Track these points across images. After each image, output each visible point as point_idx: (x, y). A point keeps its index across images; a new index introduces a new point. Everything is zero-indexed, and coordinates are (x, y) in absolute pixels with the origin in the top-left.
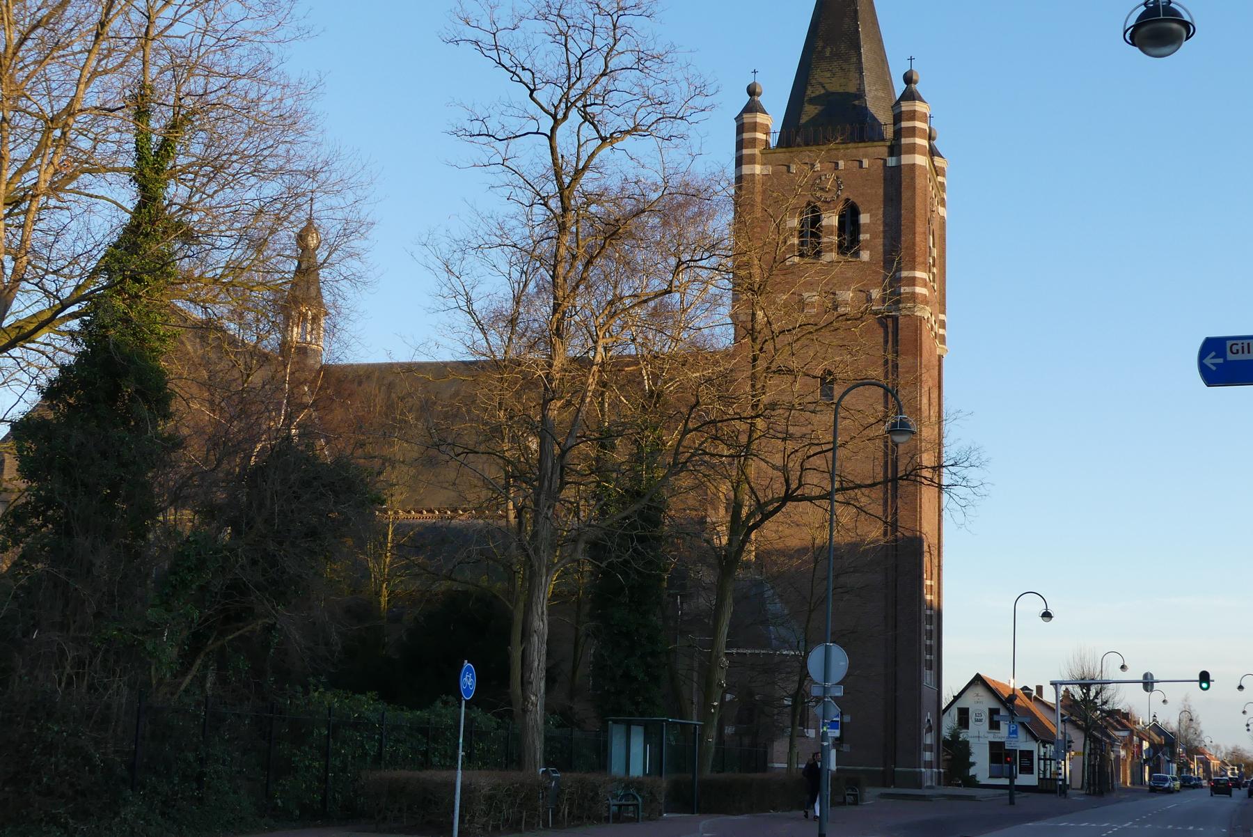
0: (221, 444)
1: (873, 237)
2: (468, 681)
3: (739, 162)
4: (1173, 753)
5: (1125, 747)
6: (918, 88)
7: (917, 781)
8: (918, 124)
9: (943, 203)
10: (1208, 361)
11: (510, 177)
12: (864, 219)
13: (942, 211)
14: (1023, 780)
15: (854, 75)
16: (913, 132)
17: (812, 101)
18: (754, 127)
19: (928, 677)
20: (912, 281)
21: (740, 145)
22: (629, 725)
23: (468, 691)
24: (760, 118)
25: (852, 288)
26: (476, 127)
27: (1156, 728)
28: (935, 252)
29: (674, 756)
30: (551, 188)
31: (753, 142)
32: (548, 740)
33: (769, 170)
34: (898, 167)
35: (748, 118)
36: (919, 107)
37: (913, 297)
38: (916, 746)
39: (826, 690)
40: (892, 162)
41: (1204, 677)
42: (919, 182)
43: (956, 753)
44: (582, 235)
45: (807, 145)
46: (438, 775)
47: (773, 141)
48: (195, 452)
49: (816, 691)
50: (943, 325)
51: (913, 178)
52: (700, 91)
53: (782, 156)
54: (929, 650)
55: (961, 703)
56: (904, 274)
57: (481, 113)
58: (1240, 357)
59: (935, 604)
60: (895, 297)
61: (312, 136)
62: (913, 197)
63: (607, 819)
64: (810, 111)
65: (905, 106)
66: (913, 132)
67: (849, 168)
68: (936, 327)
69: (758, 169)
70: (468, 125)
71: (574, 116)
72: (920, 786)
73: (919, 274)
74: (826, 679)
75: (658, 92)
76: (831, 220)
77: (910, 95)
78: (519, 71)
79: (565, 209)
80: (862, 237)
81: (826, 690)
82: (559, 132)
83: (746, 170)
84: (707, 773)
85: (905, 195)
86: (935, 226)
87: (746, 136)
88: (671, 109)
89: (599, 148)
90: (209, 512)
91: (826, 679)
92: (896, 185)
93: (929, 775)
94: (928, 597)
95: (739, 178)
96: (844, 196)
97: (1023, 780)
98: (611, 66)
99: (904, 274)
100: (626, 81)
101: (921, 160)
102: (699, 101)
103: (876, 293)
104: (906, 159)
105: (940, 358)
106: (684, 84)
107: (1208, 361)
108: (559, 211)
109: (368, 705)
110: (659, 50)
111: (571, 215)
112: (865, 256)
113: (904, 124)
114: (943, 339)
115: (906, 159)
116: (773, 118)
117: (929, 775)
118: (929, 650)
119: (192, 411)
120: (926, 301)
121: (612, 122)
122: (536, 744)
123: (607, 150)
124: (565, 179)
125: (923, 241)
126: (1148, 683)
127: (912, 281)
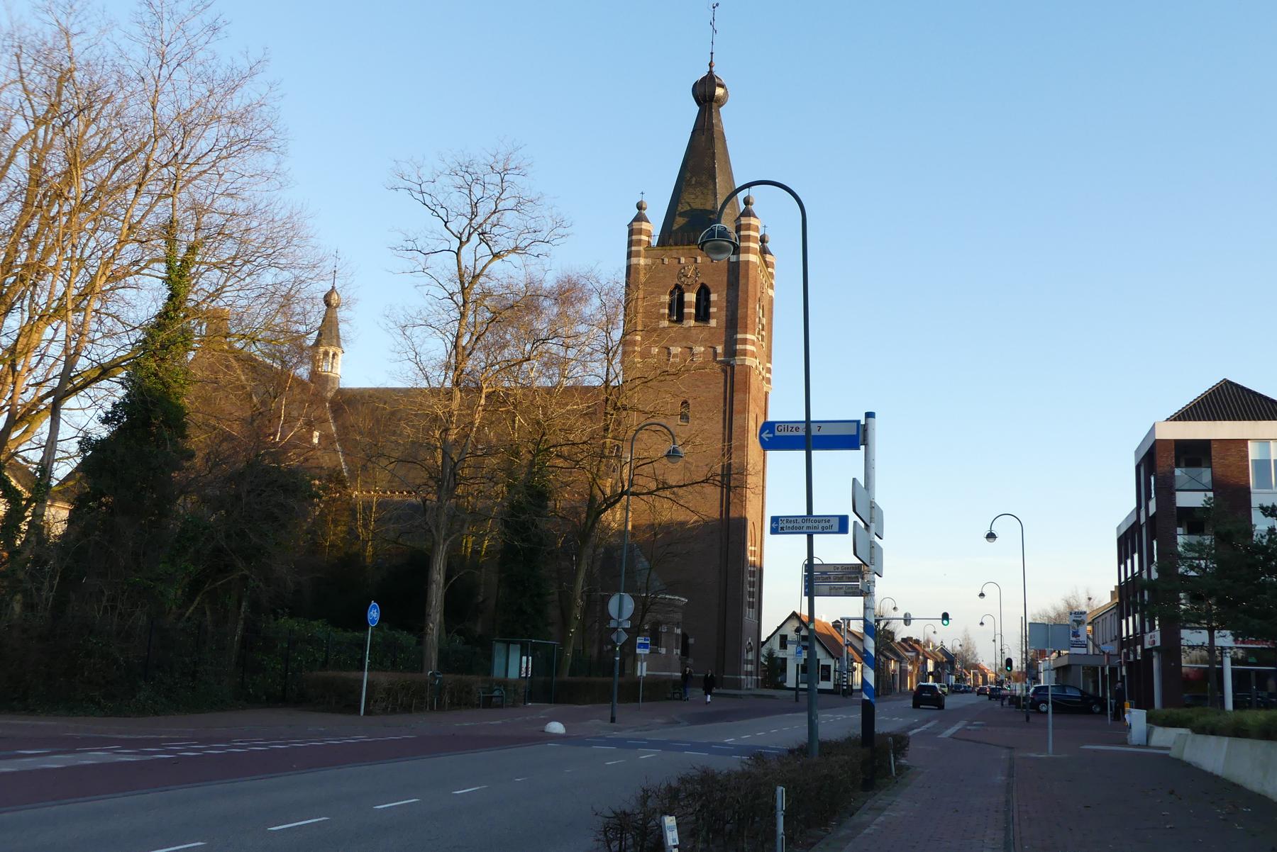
0: (214, 459)
1: (720, 309)
2: (374, 614)
3: (630, 255)
4: (953, 668)
5: (912, 663)
6: (753, 208)
7: (737, 684)
8: (752, 233)
9: (771, 286)
10: (764, 435)
11: (427, 279)
12: (713, 297)
13: (770, 291)
14: (824, 685)
15: (711, 197)
16: (748, 238)
17: (681, 215)
18: (640, 232)
19: (749, 613)
20: (745, 341)
21: (630, 244)
22: (508, 644)
23: (373, 621)
24: (644, 225)
25: (698, 345)
26: (410, 245)
27: (943, 651)
28: (764, 321)
29: (545, 663)
30: (456, 288)
31: (639, 242)
32: (440, 651)
33: (649, 261)
34: (738, 263)
35: (636, 225)
36: (753, 221)
37: (744, 353)
38: (738, 660)
39: (619, 623)
40: (733, 259)
41: (945, 616)
42: (751, 273)
43: (776, 668)
44: (492, 315)
45: (676, 244)
46: (353, 675)
47: (654, 242)
48: (198, 461)
49: (613, 624)
50: (769, 371)
51: (747, 271)
52: (559, 224)
53: (660, 252)
54: (751, 594)
55: (782, 632)
56: (739, 336)
57: (412, 236)
58: (782, 434)
59: (758, 563)
60: (731, 352)
61: (313, 241)
62: (747, 284)
63: (478, 706)
64: (680, 221)
65: (744, 221)
66: (748, 238)
67: (694, 264)
68: (764, 373)
69: (642, 261)
70: (405, 244)
71: (475, 238)
72: (740, 689)
73: (749, 336)
74: (620, 616)
75: (532, 224)
76: (691, 297)
77: (748, 213)
78: (438, 209)
79: (465, 302)
80: (713, 310)
81: (619, 623)
82: (463, 251)
83: (634, 260)
84: (566, 677)
85: (742, 282)
86: (765, 302)
87: (634, 237)
88: (540, 236)
89: (490, 262)
90: (205, 500)
91: (620, 616)
92: (736, 274)
93: (749, 681)
94: (751, 558)
95: (629, 268)
96: (700, 281)
97: (824, 685)
98: (499, 208)
99: (739, 336)
100: (509, 218)
101: (754, 258)
102: (560, 231)
103: (720, 349)
104: (743, 257)
105: (767, 393)
106: (549, 220)
107: (764, 435)
108: (461, 303)
109: (318, 628)
110: (533, 196)
111: (470, 306)
112: (713, 323)
113: (742, 233)
114: (769, 381)
115: (743, 257)
116: (655, 225)
117: (749, 681)
118: (751, 594)
119: (197, 440)
120: (753, 355)
121: (503, 244)
122: (433, 657)
123: (498, 262)
124: (467, 281)
125: (754, 311)
126: (907, 620)
127: (745, 341)
